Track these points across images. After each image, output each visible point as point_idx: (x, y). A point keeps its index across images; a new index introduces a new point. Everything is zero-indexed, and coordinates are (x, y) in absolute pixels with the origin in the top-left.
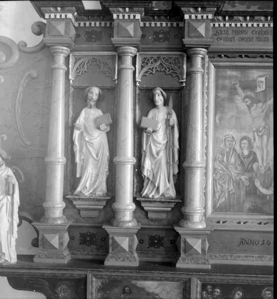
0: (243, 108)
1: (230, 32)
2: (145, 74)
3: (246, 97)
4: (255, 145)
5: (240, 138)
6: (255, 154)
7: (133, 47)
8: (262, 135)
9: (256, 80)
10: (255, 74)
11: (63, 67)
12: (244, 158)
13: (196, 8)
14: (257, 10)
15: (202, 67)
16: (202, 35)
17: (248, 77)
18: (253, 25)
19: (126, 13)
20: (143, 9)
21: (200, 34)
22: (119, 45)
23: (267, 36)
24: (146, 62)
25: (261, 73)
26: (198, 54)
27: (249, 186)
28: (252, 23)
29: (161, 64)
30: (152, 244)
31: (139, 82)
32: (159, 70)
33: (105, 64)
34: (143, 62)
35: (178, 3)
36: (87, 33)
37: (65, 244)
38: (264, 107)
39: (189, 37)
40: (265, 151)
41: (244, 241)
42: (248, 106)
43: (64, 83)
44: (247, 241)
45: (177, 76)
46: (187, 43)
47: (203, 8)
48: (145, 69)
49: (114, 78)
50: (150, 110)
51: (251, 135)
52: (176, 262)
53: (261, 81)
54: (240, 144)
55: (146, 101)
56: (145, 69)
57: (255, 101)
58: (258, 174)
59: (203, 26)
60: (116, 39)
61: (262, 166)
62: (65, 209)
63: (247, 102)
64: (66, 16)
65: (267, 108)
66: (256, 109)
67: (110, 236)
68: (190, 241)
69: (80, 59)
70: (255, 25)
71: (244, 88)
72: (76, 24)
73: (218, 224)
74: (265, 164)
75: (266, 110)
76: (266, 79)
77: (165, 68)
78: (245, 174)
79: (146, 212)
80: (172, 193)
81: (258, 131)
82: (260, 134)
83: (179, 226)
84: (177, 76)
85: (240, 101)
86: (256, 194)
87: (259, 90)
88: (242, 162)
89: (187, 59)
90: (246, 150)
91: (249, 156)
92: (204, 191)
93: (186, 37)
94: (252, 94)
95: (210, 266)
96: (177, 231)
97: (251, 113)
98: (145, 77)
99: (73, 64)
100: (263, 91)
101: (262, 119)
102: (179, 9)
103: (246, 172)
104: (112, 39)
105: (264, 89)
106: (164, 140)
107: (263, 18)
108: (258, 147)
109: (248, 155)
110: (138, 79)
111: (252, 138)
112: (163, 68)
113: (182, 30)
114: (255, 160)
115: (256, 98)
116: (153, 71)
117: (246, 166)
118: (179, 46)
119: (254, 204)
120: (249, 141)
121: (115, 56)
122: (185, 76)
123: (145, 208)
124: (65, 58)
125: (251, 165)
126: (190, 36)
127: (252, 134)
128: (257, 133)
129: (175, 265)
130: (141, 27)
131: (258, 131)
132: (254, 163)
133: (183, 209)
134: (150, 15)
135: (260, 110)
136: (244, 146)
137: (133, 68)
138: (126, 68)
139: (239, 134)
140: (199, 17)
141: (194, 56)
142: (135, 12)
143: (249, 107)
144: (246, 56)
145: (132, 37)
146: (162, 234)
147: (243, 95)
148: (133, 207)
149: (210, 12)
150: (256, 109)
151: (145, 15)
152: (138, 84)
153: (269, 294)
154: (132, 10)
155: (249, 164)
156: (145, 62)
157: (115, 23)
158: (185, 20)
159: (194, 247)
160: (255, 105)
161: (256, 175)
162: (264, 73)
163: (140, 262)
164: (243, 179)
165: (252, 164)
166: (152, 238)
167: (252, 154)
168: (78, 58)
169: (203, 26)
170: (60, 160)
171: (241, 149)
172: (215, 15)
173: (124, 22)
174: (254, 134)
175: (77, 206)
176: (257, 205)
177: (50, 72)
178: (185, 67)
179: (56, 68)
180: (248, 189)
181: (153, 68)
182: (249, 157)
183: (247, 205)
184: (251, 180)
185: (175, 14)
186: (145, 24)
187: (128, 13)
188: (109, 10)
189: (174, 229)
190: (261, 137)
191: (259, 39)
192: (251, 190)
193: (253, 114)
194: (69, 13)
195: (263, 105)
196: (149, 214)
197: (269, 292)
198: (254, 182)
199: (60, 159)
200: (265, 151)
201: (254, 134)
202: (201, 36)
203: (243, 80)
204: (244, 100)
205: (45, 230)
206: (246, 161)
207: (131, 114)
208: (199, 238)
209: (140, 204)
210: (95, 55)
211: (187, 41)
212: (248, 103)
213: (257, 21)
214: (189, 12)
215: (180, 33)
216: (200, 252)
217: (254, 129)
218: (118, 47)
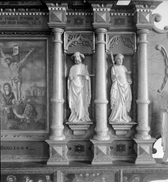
2: (71, 45)
3: (6, 59)
4: (13, 88)
5: (3, 84)
6: (13, 94)
7: (148, 29)
9: (13, 48)
10: (12, 45)
11: (60, 42)
12: (6, 96)
13: (101, 5)
14: (8, 5)
16: (103, 20)
17: (8, 46)
19: (56, 7)
21: (103, 19)
23: (15, 21)
24: (71, 37)
25: (15, 44)
26: (57, 32)
29: (80, 39)
30: (77, 150)
34: (69, 38)
37: (66, 153)
38: (18, 65)
40: (19, 92)
44: (8, 147)
46: (138, 27)
47: (105, 5)
48: (70, 42)
51: (10, 82)
54: (4, 88)
55: (70, 60)
56: (70, 42)
57: (12, 61)
60: (51, 23)
63: (7, 62)
64: (62, 9)
65: (20, 65)
66: (13, 66)
67: (95, 146)
69: (112, 37)
70: (7, 14)
71: (5, 53)
72: (67, 14)
73: (15, 137)
74: (19, 100)
75: (19, 66)
76: (19, 47)
78: (7, 106)
79: (73, 131)
81: (14, 79)
82: (16, 81)
83: (134, 138)
85: (4, 61)
86: (14, 118)
87: (15, 54)
88: (5, 99)
90: (8, 91)
91: (9, 95)
92: (51, 115)
93: (94, 22)
94: (11, 57)
95: (112, 162)
96: (47, 142)
97: (10, 69)
98: (71, 47)
100: (17, 55)
101: (17, 72)
104: (48, 23)
105: (17, 54)
106: (82, 84)
107: (10, 10)
108: (15, 89)
109: (9, 94)
110: (66, 48)
111: (11, 84)
112: (81, 41)
113: (92, 17)
114: (13, 97)
116: (75, 43)
118: (90, 28)
119: (13, 124)
120: (9, 86)
121: (134, 34)
122: (94, 47)
123: (71, 128)
124: (62, 36)
125: (10, 101)
126: (141, 21)
127: (11, 82)
129: (46, 164)
130: (67, 15)
131: (14, 79)
133: (95, 129)
134: (72, 8)
135: (16, 67)
136: (6, 89)
137: (62, 42)
138: (143, 43)
139: (3, 82)
140: (57, 9)
142: (106, 8)
143: (9, 65)
144: (17, 33)
145: (60, 22)
148: (63, 127)
151: (68, 8)
153: (11, 179)
156: (70, 37)
157: (50, 13)
158: (94, 11)
160: (12, 64)
161: (14, 107)
162: (18, 44)
163: (69, 162)
164: (6, 110)
165: (12, 100)
166: (77, 147)
167: (11, 93)
170: (61, 101)
172: (112, 8)
173: (100, 12)
174: (12, 81)
175: (114, 129)
176: (15, 125)
177: (53, 45)
178: (94, 40)
180: (9, 115)
181: (75, 41)
183: (9, 125)
184: (11, 110)
185: (87, 8)
186: (68, 14)
188: (46, 5)
189: (89, 141)
190: (17, 83)
191: (9, 23)
193: (11, 69)
194: (63, 7)
195: (17, 63)
197: (11, 178)
198: (13, 111)
200: (19, 92)
201: (12, 81)
202: (103, 21)
206: (8, 98)
207: (61, 68)
209: (69, 126)
211: (95, 24)
212: (8, 62)
213: (7, 12)
214: (51, 6)
215: (90, 18)
217: (12, 78)
218: (51, 28)
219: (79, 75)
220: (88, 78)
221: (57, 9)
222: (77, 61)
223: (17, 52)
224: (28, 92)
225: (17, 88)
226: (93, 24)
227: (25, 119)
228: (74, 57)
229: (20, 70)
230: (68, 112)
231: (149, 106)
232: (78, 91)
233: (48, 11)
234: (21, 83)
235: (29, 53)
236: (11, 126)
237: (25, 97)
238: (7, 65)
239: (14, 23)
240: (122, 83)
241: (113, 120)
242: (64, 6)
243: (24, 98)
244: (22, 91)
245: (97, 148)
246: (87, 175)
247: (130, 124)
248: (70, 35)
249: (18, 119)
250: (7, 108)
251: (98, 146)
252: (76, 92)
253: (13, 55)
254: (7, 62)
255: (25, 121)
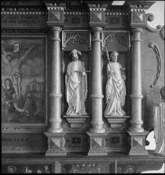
0: (6, 62)
1: (34, 17)
2: (69, 43)
3: (8, 56)
4: (13, 83)
8: (18, 77)
10: (13, 42)
11: (58, 40)
12: (7, 91)
15: (60, 38)
18: (6, 13)
19: (55, 7)
20: (65, 4)
22: (52, 26)
24: (68, 35)
25: (16, 42)
27: (11, 107)
28: (45, 12)
29: (77, 37)
30: (74, 142)
31: (64, 48)
32: (76, 40)
33: (123, 37)
34: (67, 36)
35: (86, 2)
36: (111, 19)
38: (18, 61)
39: (93, 20)
41: (4, 139)
42: (9, 61)
43: (59, 49)
45: (87, 44)
49: (129, 46)
50: (69, 62)
51: (11, 78)
52: (45, 153)
53: (16, 46)
54: (5, 83)
55: (67, 57)
56: (68, 41)
57: (13, 58)
58: (16, 101)
59: (101, 14)
61: (18, 95)
62: (62, 122)
63: (8, 58)
64: (60, 9)
65: (20, 62)
66: (14, 63)
68: (54, 140)
69: (108, 35)
71: (7, 50)
74: (19, 95)
76: (19, 45)
77: (80, 39)
78: (8, 100)
79: (70, 124)
80: (85, 113)
81: (15, 75)
84: (87, 44)
85: (5, 58)
87: (15, 51)
89: (130, 35)
94: (12, 54)
99: (104, 38)
100: (17, 52)
101: (17, 69)
102: (129, 6)
103: (8, 99)
104: (47, 22)
106: (79, 80)
109: (9, 89)
111: (12, 79)
114: (14, 92)
115: (13, 56)
117: (9, 96)
122: (91, 45)
123: (69, 122)
126: (134, 21)
128: (15, 76)
130: (64, 15)
131: (15, 75)
132: (13, 93)
134: (69, 8)
137: (60, 40)
141: (137, 33)
143: (10, 61)
146: (79, 136)
147: (6, 54)
148: (60, 120)
149: (104, 7)
150: (14, 63)
152: (63, 49)
153: (11, 170)
154: (58, 5)
155: (11, 94)
156: (68, 35)
157: (49, 13)
158: (90, 11)
159: (56, 144)
161: (15, 101)
164: (7, 104)
165: (12, 94)
167: (12, 88)
168: (106, 34)
169: (101, 14)
170: (59, 96)
171: (6, 86)
179: (55, 40)
180: (10, 109)
181: (73, 39)
182: (11, 90)
183: (10, 118)
184: (12, 104)
186: (66, 13)
187: (16, 12)
191: (10, 22)
192: (11, 110)
193: (12, 65)
196: (111, 125)
198: (13, 105)
199: (58, 95)
202: (99, 20)
203: (6, 45)
204: (6, 57)
205: (94, 136)
206: (9, 93)
208: (59, 138)
209: (66, 119)
210: (117, 33)
212: (9, 59)
214: (50, 6)
215: (45, 17)
216: (101, 146)
217: (13, 74)
219: (76, 72)
220: (84, 74)
221: (55, 8)
222: (74, 58)
223: (18, 50)
224: (28, 87)
225: (17, 83)
226: (89, 23)
227: (25, 112)
228: (72, 55)
229: (20, 67)
230: (65, 106)
231: (142, 100)
232: (75, 86)
233: (47, 11)
234: (21, 78)
235: (29, 51)
236: (11, 119)
237: (24, 91)
238: (8, 62)
239: (15, 22)
240: (117, 78)
241: (108, 114)
242: (62, 6)
243: (24, 92)
244: (22, 85)
245: (93, 140)
246: (84, 165)
247: (124, 118)
248: (68, 34)
249: (19, 113)
250: (8, 102)
251: (134, 138)
252: (74, 87)
253: (14, 52)
254: (8, 58)
255: (25, 115)
